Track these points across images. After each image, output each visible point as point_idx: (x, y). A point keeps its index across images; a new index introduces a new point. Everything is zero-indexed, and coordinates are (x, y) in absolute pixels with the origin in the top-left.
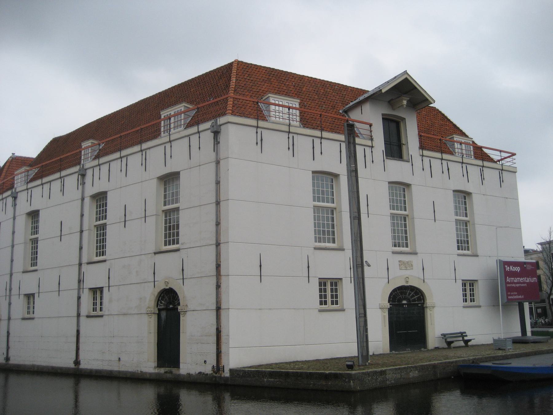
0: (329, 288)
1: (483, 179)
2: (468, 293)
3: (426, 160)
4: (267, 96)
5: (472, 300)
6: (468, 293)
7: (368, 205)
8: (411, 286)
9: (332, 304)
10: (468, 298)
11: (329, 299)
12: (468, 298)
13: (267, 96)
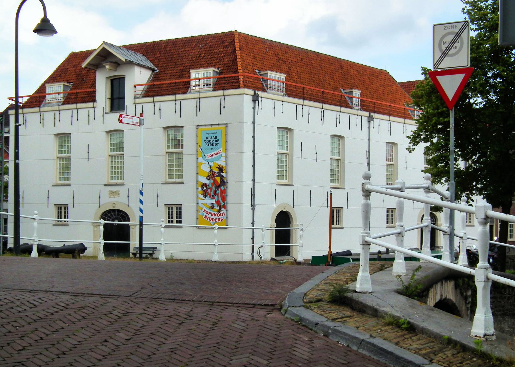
0: (175, 211)
1: (390, 130)
2: (390, 217)
3: (359, 117)
4: (266, 72)
5: (392, 223)
6: (390, 217)
7: (254, 151)
8: (117, 210)
9: (177, 222)
10: (390, 221)
11: (175, 219)
12: (390, 221)
13: (266, 72)
